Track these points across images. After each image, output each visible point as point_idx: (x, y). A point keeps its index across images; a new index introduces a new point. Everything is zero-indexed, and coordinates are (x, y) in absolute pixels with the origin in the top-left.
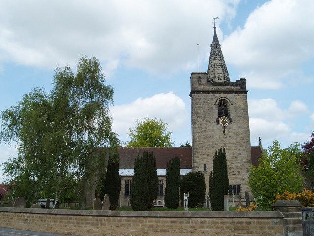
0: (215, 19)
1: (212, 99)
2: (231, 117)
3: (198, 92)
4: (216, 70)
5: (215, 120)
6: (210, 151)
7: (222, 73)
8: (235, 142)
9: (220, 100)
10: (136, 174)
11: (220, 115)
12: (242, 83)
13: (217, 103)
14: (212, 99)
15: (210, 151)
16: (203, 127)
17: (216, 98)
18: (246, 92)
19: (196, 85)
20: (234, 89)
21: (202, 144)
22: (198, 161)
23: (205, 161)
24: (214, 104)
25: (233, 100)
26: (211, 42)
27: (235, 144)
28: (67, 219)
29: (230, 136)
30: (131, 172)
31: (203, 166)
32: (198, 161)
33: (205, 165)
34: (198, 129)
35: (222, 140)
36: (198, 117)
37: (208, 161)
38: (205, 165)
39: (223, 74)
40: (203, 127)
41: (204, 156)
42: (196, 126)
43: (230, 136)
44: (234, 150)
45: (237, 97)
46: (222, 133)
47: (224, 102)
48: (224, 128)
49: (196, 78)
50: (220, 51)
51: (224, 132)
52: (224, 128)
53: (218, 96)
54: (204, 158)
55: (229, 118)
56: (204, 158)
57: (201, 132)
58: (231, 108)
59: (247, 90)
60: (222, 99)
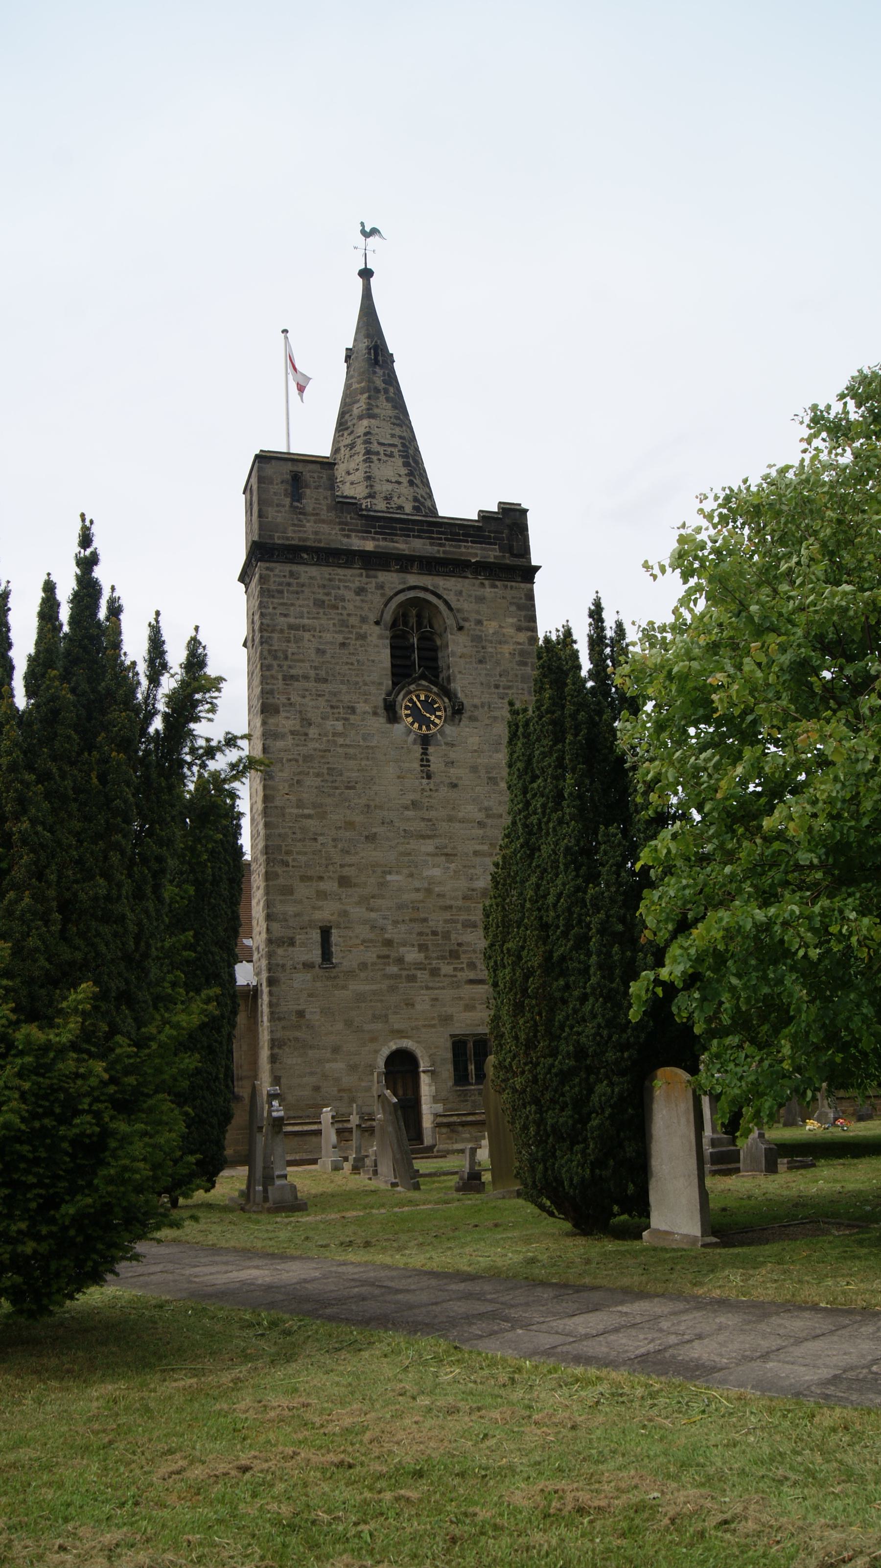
0: (366, 234)
1: (360, 591)
2: (457, 686)
3: (293, 553)
4: (375, 465)
5: (378, 699)
6: (348, 859)
7: (405, 480)
8: (480, 816)
9: (401, 598)
10: (231, 967)
11: (401, 673)
12: (507, 526)
13: (388, 617)
14: (360, 591)
15: (348, 859)
16: (313, 732)
17: (380, 587)
18: (529, 573)
19: (278, 516)
20: (475, 552)
21: (309, 822)
22: (291, 909)
23: (326, 913)
24: (372, 617)
25: (466, 605)
26: (345, 333)
27: (481, 825)
28: (337, 608)
29: (454, 786)
30: (799, 778)
31: (316, 935)
32: (291, 909)
33: (326, 933)
34: (289, 741)
35: (415, 805)
36: (289, 679)
37: (345, 913)
38: (326, 933)
39: (411, 483)
40: (313, 732)
41: (323, 886)
42: (286, 722)
43: (454, 786)
44: (476, 853)
45: (488, 592)
46: (416, 765)
47: (419, 616)
48: (425, 741)
49: (278, 480)
50: (392, 380)
51: (425, 762)
52: (425, 741)
53: (391, 579)
54: (322, 895)
55: (447, 692)
56: (322, 895)
57: (307, 758)
58: (456, 648)
59: (534, 562)
60: (411, 594)
